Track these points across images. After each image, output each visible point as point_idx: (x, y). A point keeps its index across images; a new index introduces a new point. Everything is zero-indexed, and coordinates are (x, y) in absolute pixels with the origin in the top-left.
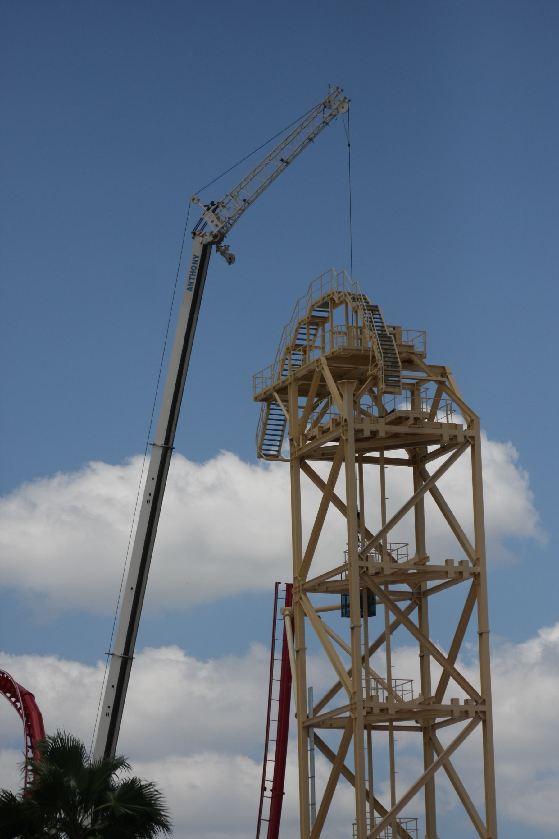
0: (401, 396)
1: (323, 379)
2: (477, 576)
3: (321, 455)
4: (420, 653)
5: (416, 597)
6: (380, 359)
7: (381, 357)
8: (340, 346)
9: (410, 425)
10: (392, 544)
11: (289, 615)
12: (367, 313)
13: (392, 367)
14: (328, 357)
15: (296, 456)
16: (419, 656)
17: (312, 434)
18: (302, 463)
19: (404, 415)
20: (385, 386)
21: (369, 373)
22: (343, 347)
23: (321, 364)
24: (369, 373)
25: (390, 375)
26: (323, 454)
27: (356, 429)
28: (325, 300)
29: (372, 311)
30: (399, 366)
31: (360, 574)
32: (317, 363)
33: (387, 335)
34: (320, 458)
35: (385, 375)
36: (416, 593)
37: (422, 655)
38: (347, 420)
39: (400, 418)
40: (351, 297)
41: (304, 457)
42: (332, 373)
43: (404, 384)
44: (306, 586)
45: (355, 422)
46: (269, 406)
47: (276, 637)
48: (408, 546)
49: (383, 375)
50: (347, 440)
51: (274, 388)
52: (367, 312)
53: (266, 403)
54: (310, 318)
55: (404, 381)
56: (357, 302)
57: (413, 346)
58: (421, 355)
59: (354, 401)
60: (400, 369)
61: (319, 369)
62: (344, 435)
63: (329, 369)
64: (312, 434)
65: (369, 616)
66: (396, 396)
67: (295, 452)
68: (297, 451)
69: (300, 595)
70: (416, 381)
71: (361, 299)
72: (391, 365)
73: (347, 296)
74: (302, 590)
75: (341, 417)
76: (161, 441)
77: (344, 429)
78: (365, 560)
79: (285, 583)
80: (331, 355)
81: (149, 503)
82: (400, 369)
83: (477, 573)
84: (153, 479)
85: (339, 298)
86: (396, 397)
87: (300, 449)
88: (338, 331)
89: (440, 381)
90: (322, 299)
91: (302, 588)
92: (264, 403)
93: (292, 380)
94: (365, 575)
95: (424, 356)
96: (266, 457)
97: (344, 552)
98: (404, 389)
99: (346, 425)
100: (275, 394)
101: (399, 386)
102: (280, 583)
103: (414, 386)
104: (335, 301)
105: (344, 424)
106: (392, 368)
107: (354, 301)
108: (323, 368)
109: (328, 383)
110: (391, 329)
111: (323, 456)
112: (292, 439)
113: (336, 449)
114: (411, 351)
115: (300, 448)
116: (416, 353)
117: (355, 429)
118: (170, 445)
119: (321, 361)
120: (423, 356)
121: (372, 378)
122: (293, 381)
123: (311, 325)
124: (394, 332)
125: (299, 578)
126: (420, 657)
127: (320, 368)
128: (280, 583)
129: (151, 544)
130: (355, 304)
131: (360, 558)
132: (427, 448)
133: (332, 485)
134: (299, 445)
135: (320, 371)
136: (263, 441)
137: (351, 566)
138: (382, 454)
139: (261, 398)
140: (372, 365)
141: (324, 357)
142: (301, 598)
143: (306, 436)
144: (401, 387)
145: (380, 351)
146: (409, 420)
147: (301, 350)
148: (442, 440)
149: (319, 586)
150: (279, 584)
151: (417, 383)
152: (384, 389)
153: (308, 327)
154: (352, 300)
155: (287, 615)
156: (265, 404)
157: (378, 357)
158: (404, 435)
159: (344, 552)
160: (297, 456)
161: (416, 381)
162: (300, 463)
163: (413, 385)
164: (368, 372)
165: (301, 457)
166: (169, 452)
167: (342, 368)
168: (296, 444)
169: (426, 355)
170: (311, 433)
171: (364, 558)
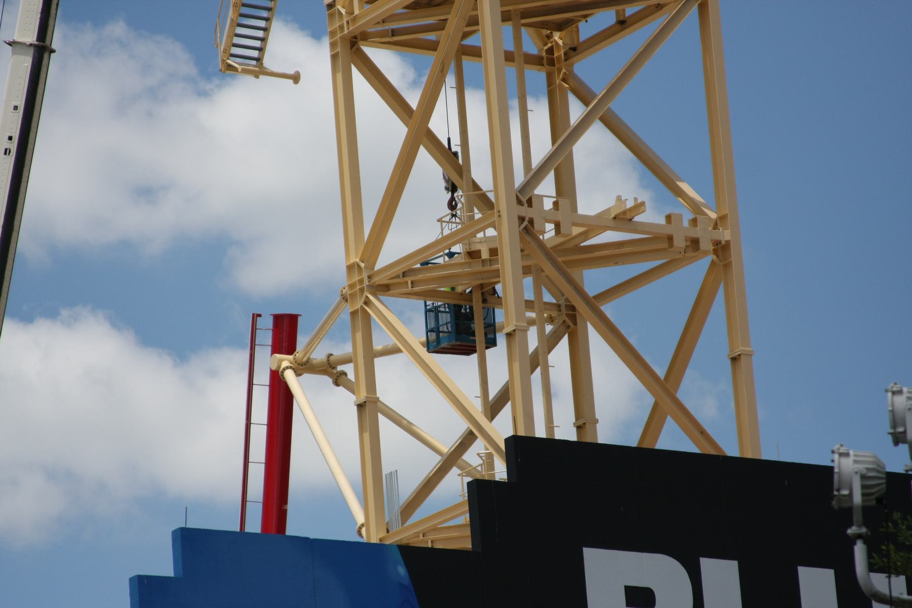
2: (722, 249)
3: (390, 34)
4: (576, 421)
5: (567, 315)
11: (291, 368)
16: (574, 426)
18: (355, 48)
31: (519, 231)
34: (387, 39)
36: (566, 305)
37: (580, 423)
44: (377, 280)
47: (253, 419)
65: (487, 348)
68: (348, 23)
69: (364, 296)
74: (368, 286)
76: (31, 37)
78: (526, 205)
79: (271, 315)
81: (9, 155)
83: (723, 242)
84: (16, 108)
87: (355, 19)
91: (369, 282)
94: (528, 233)
97: (439, 221)
102: (260, 315)
111: (393, 35)
118: (47, 42)
125: (362, 265)
126: (575, 428)
128: (260, 315)
129: (14, 234)
131: (520, 202)
133: (442, 71)
136: (232, 38)
137: (500, 216)
142: (367, 302)
149: (403, 276)
150: (258, 318)
155: (287, 368)
159: (439, 221)
160: (348, 32)
162: (351, 49)
166: (46, 56)
171: (524, 200)
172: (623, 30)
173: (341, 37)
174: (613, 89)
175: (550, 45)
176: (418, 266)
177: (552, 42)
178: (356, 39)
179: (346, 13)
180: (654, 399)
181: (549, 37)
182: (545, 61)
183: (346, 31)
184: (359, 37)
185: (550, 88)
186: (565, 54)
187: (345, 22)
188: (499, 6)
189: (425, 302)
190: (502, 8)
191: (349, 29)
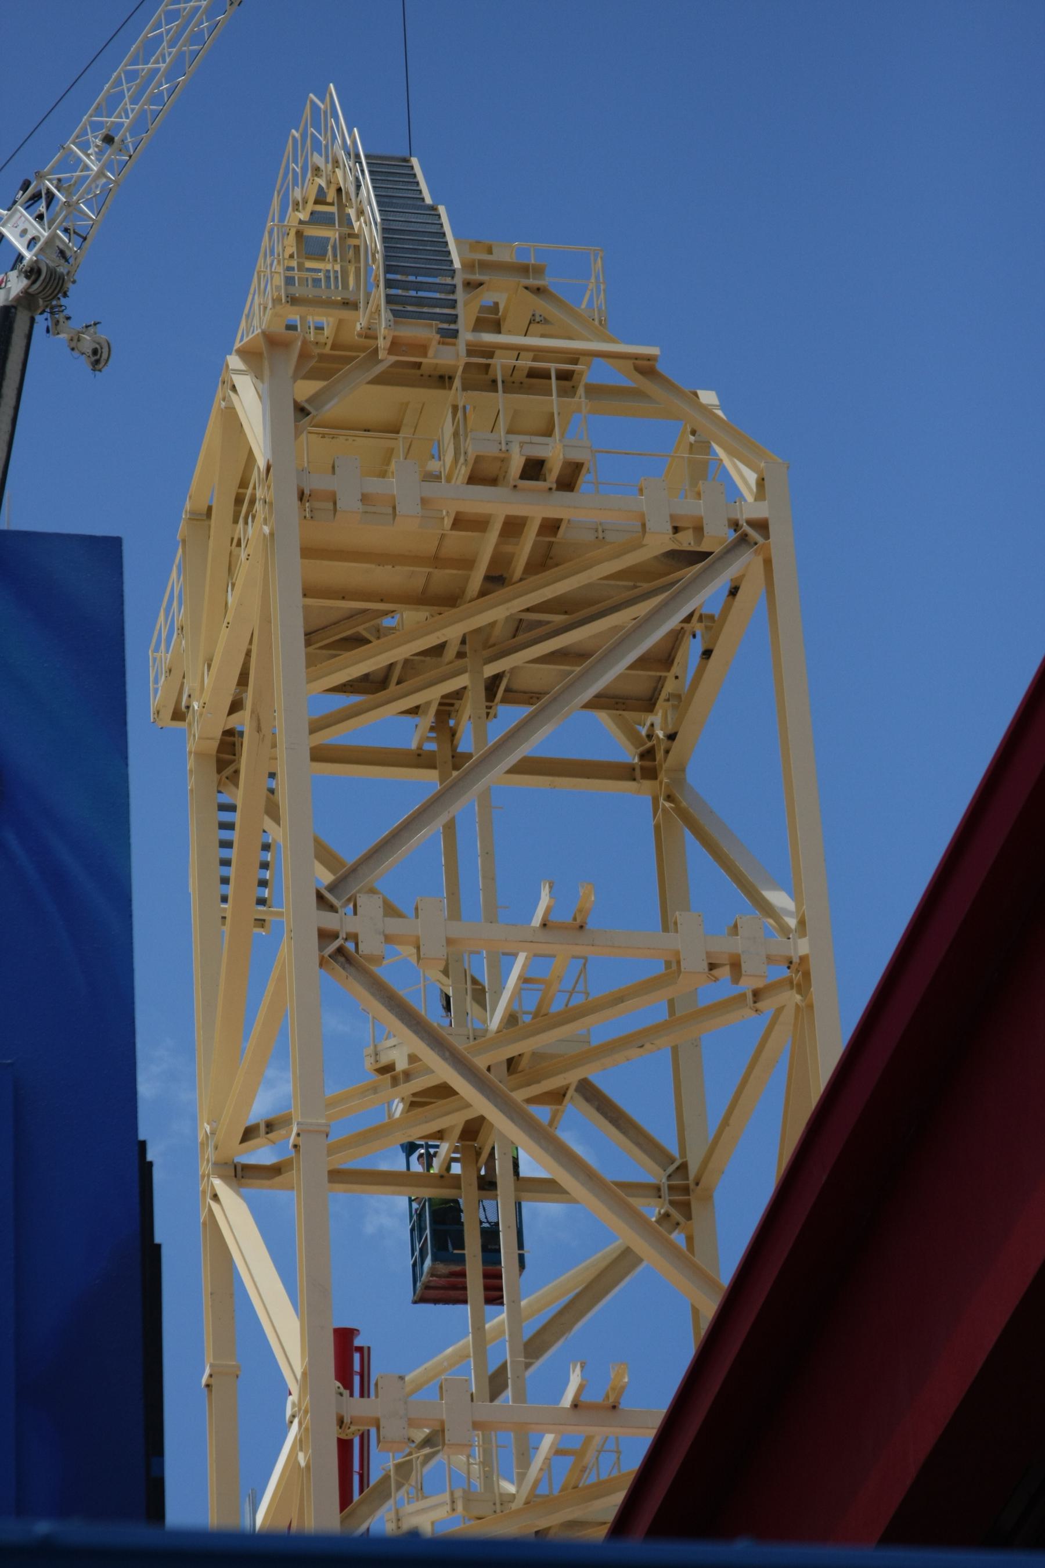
33: (423, 199)
108: (234, 388)
182: (638, 772)
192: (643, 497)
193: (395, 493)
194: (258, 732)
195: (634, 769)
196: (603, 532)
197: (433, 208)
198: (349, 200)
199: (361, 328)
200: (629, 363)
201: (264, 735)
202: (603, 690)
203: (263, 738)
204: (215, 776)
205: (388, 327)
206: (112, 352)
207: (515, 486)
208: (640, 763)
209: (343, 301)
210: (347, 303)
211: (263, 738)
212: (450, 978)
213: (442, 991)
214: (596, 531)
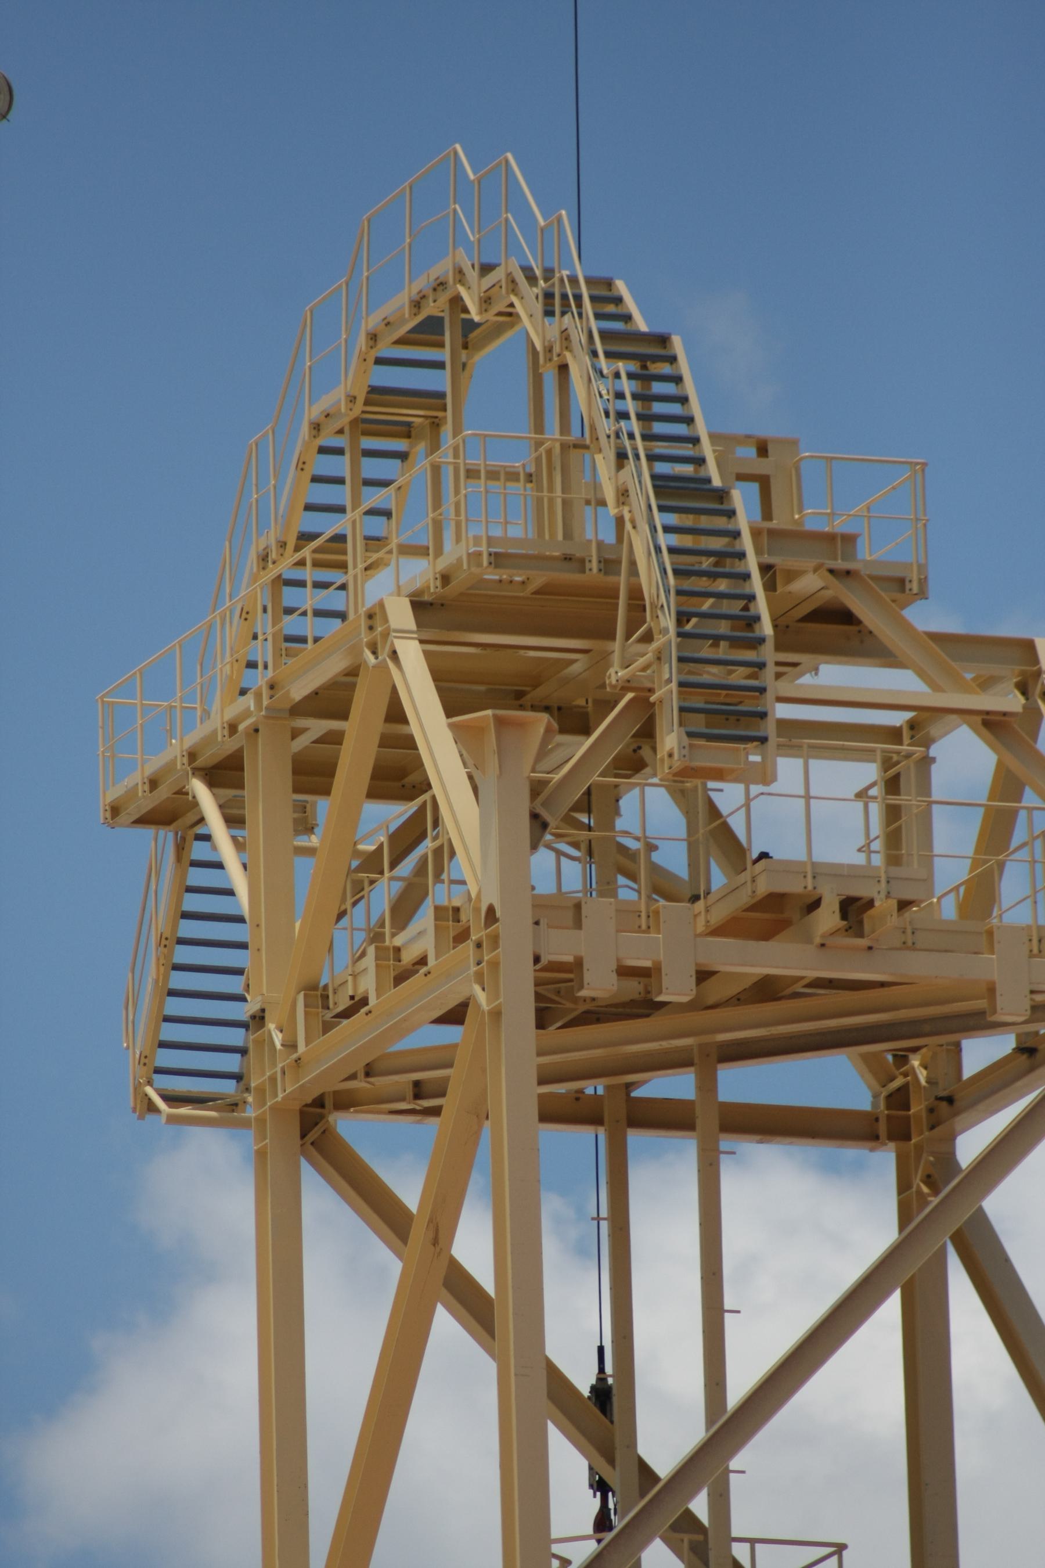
0: (773, 788)
1: (396, 714)
3: (410, 1094)
6: (662, 606)
7: (667, 592)
8: (477, 540)
9: (823, 936)
10: (758, 1546)
12: (605, 371)
13: (736, 643)
14: (426, 598)
15: (279, 1099)
17: (355, 986)
19: (793, 886)
20: (686, 741)
21: (616, 674)
22: (489, 545)
23: (386, 635)
24: (616, 674)
25: (724, 682)
26: (417, 1084)
27: (544, 961)
28: (430, 309)
29: (644, 360)
30: (762, 640)
32: (371, 628)
33: (709, 481)
35: (681, 684)
38: (498, 914)
39: (775, 901)
40: (535, 290)
41: (319, 1102)
42: (438, 676)
43: (785, 726)
45: (537, 923)
46: (181, 848)
48: (845, 1553)
49: (674, 686)
50: (496, 1014)
51: (192, 756)
52: (603, 362)
53: (171, 836)
54: (361, 400)
55: (783, 711)
56: (563, 314)
57: (849, 540)
58: (901, 583)
59: (535, 816)
60: (768, 653)
61: (377, 658)
62: (483, 989)
63: (427, 654)
64: (355, 986)
66: (755, 789)
67: (273, 1079)
70: (909, 715)
71: (578, 298)
72: (729, 633)
73: (520, 285)
75: (473, 895)
77: (486, 958)
80: (434, 587)
82: (768, 653)
85: (486, 301)
86: (752, 794)
88: (798, 470)
89: (988, 713)
90: (411, 301)
92: (162, 832)
93: (263, 713)
95: (915, 590)
96: (170, 1107)
98: (789, 749)
99: (495, 940)
100: (200, 790)
101: (764, 740)
103: (901, 743)
104: (466, 310)
105: (483, 933)
106: (731, 646)
107: (549, 313)
108: (394, 655)
109: (414, 728)
110: (751, 452)
111: (417, 1096)
112: (263, 1010)
113: (450, 1065)
114: (840, 564)
115: (295, 1056)
116: (864, 572)
117: (537, 959)
119: (386, 620)
120: (908, 586)
121: (631, 701)
122: (266, 717)
123: (366, 433)
124: (762, 466)
127: (384, 655)
130: (553, 328)
132: (958, 1048)
134: (291, 1045)
135: (382, 667)
138: (708, 1085)
139: (135, 810)
140: (628, 636)
141: (406, 597)
143: (325, 997)
144: (773, 740)
145: (663, 563)
146: (820, 910)
147: (309, 562)
148: (994, 1012)
151: (912, 725)
152: (676, 756)
153: (354, 442)
154: (539, 307)
156: (167, 837)
157: (654, 591)
158: (806, 986)
160: (283, 1098)
161: (909, 715)
162: (303, 1136)
163: (894, 734)
164: (612, 671)
165: (306, 1105)
167: (522, 652)
168: (278, 1038)
169: (923, 582)
170: (350, 978)
172: (1032, 1069)
173: (271, 1108)
174: (352, 934)
175: (899, 1082)
176: (615, 1499)
177: (906, 1075)
178: (323, 1106)
179: (282, 1045)
180: (775, 857)
181: (901, 1059)
182: (882, 1128)
183: (280, 1096)
184: (329, 1103)
185: (902, 1196)
186: (931, 1110)
187: (278, 1069)
188: (377, 745)
189: (1001, 921)
190: (388, 725)
191: (285, 1091)
192: (994, 956)
193: (662, 958)
194: (434, 1245)
195: (877, 1120)
196: (913, 933)
197: (722, 495)
198: (655, 618)
199: (617, 681)
200: (978, 719)
201: (441, 1249)
202: (625, 302)
203: (440, 1252)
204: (299, 1142)
205: (682, 759)
206: (15, 98)
207: (823, 945)
208: (886, 1112)
209: (565, 556)
210: (570, 559)
211: (440, 1252)
212: (618, 1468)
213: (250, 689)
214: (904, 932)
